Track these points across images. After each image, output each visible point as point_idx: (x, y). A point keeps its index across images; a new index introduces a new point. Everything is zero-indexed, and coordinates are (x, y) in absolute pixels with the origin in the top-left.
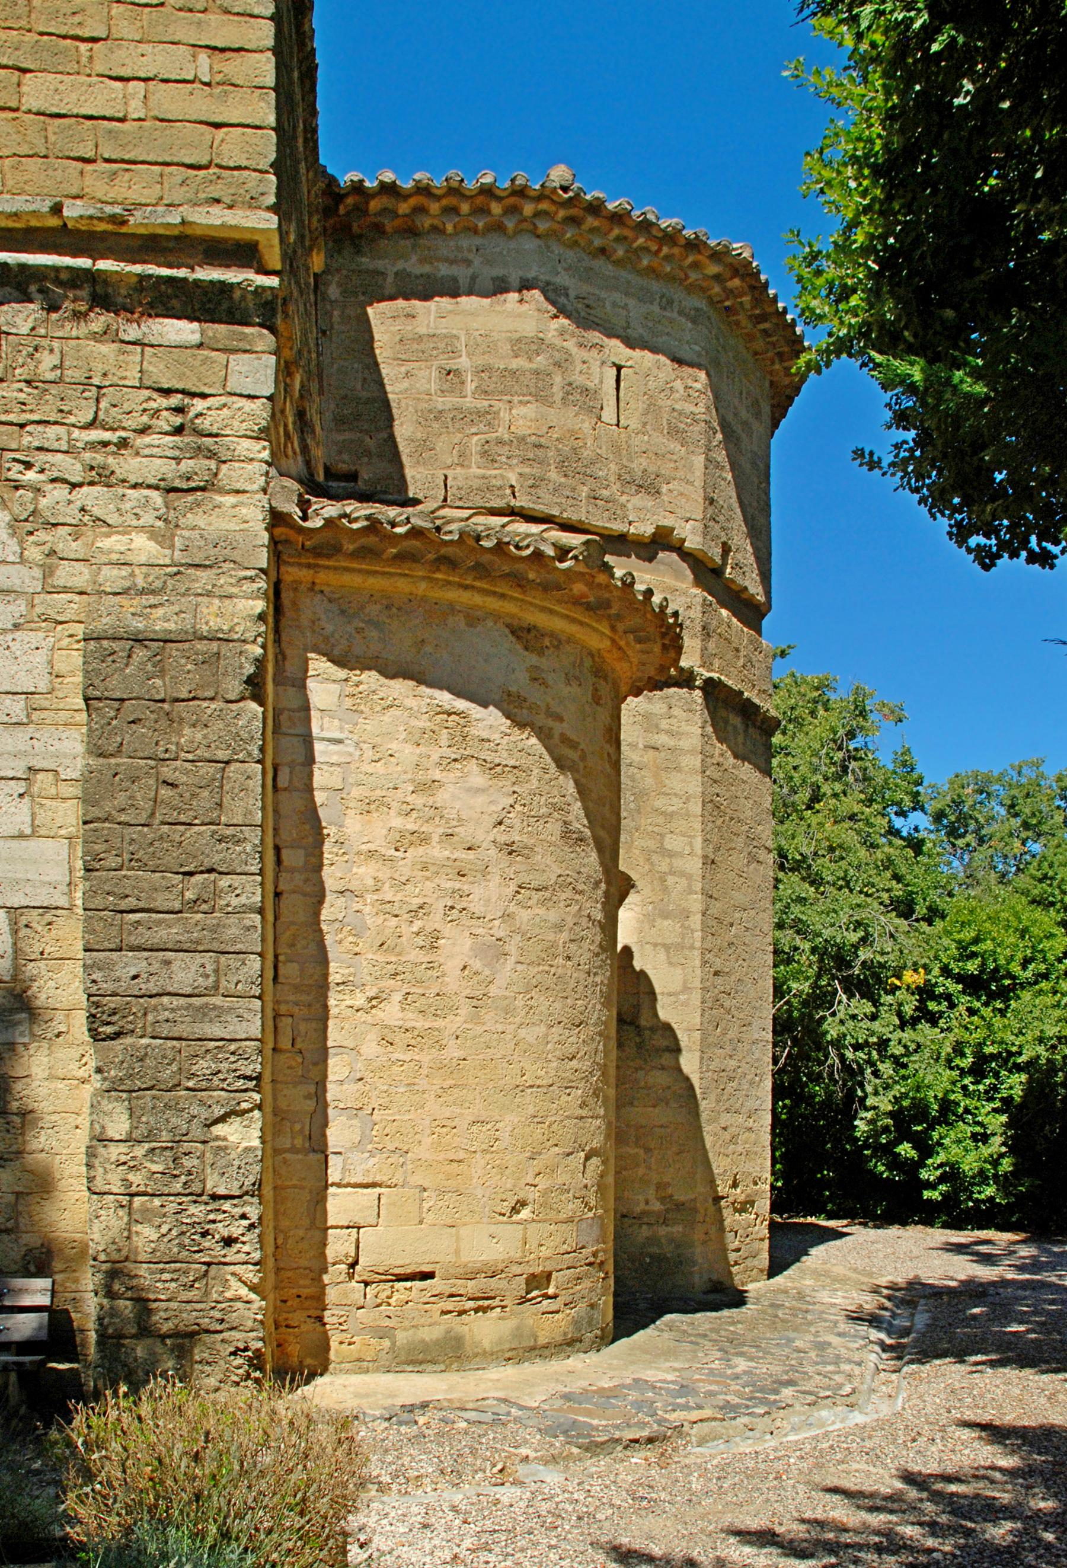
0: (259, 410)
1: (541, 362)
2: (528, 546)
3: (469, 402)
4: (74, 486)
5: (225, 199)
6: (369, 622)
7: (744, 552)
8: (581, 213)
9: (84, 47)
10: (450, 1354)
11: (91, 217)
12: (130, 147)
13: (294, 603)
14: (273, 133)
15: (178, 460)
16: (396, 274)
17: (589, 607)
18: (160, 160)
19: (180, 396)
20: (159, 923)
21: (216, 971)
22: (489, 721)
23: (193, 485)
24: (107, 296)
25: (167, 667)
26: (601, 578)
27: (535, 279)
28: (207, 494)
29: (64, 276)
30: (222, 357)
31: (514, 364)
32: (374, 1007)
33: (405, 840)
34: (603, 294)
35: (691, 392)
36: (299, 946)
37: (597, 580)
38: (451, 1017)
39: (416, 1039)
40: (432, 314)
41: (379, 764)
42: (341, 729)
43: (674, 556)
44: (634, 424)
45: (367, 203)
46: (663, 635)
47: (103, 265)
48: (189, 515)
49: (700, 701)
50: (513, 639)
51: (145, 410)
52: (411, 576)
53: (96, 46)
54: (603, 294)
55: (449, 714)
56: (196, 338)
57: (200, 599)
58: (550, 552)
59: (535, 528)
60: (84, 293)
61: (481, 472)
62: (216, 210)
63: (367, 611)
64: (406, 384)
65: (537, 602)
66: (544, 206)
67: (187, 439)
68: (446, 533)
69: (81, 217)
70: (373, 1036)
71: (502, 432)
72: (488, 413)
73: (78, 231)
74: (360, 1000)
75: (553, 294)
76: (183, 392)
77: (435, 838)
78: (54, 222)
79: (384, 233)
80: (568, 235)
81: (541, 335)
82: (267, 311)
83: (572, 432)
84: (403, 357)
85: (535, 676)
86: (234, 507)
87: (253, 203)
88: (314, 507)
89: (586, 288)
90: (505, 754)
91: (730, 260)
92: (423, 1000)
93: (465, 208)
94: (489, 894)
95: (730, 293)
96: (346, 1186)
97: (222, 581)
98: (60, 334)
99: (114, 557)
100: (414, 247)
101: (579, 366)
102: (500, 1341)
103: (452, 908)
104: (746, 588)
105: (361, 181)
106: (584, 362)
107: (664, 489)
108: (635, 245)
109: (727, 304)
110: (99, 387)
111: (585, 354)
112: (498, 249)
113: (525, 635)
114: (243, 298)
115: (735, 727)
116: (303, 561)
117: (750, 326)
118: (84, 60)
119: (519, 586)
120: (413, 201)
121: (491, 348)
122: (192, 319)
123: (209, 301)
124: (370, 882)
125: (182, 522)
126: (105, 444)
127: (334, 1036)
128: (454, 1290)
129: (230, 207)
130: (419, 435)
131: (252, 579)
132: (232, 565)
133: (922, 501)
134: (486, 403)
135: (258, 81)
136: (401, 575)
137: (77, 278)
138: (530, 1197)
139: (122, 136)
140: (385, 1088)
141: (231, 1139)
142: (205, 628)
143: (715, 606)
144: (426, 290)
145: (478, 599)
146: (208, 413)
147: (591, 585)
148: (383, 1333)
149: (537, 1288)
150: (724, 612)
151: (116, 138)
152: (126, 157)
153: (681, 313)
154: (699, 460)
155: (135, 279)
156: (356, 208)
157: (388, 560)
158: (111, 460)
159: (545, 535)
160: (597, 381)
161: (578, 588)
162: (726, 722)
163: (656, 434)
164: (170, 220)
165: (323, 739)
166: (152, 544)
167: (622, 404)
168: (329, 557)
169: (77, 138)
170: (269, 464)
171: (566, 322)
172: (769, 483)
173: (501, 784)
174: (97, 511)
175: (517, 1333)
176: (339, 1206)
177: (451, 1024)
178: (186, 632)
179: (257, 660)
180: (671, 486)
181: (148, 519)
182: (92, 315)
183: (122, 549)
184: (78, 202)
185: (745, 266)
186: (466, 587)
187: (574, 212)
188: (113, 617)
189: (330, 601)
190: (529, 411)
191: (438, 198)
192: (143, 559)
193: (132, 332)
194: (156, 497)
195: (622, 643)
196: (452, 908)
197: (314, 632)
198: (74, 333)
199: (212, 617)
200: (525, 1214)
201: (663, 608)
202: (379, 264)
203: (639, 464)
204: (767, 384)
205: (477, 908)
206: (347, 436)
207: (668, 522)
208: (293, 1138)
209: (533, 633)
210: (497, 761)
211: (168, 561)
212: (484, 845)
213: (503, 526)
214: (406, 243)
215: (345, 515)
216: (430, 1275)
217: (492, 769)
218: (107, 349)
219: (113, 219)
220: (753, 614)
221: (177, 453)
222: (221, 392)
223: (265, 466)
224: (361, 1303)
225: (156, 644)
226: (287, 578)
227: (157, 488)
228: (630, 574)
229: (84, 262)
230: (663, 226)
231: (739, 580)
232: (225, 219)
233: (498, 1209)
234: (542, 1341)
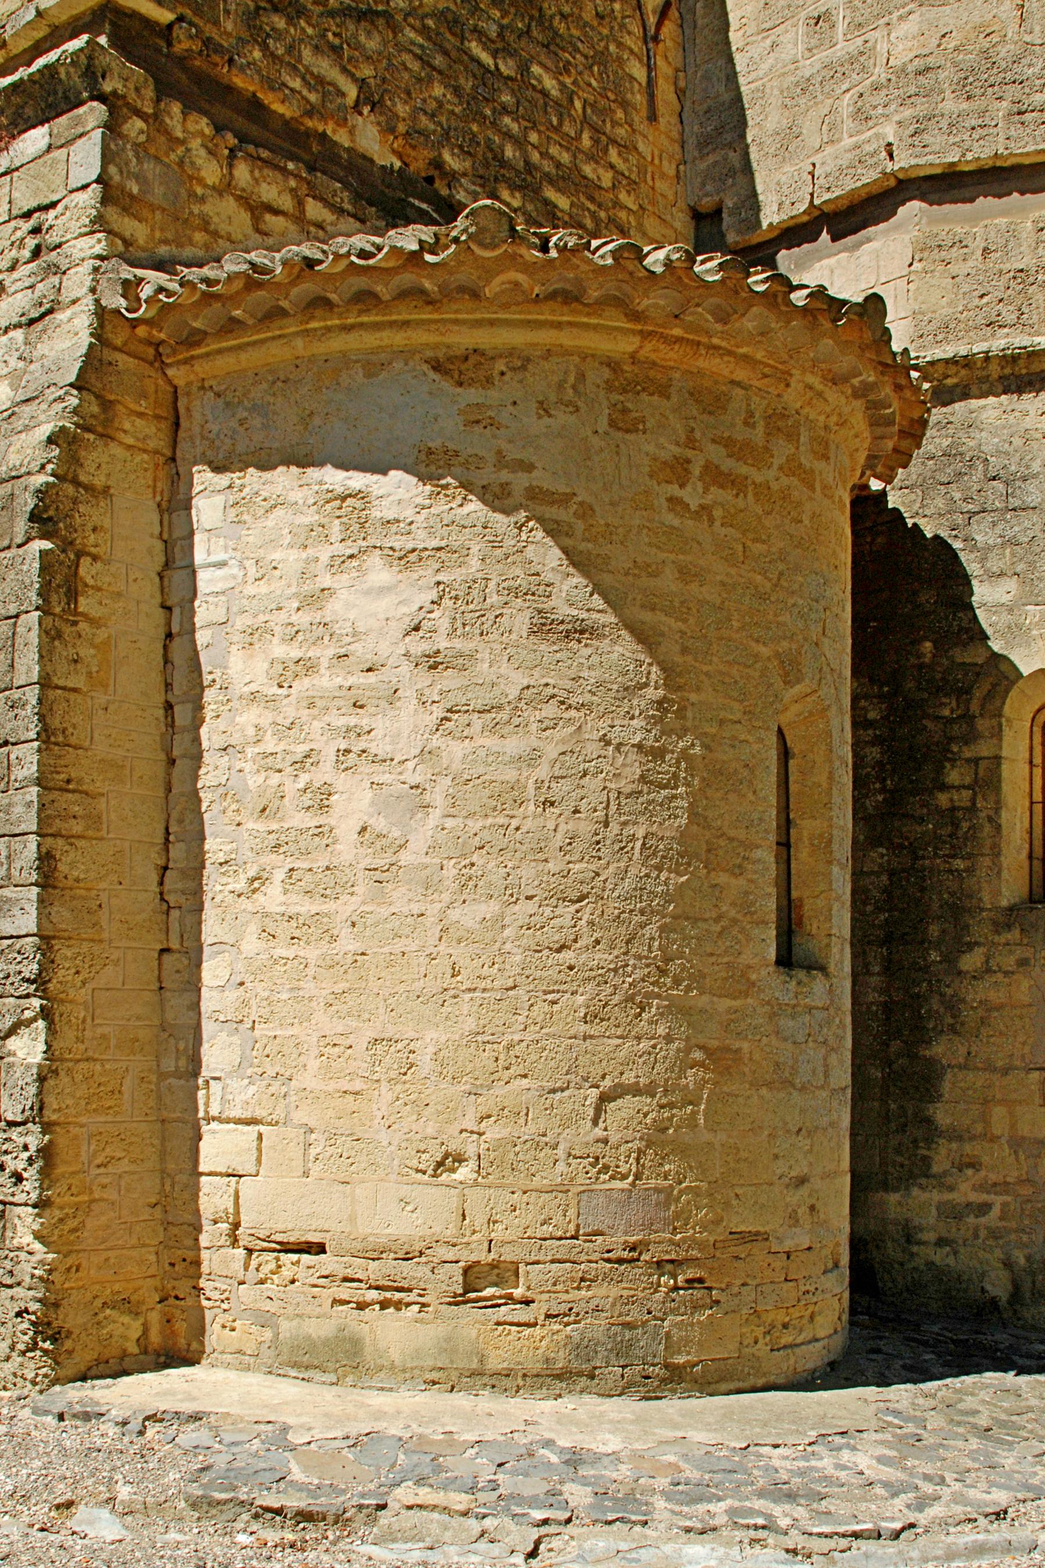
6: (254, 408)
10: (341, 1360)
13: (188, 409)
22: (396, 491)
32: (257, 889)
33: (286, 674)
36: (187, 821)
38: (344, 898)
39: (301, 928)
41: (262, 582)
55: (344, 499)
70: (253, 928)
71: (879, 73)
72: (862, 53)
74: (241, 885)
77: (324, 663)
83: (978, 28)
84: (767, 26)
86: (70, 320)
90: (421, 534)
92: (308, 876)
94: (400, 729)
96: (228, 1121)
102: (417, 1353)
103: (347, 751)
116: (181, 357)
124: (251, 731)
127: (212, 929)
128: (349, 1273)
138: (471, 1151)
140: (266, 994)
145: (371, 340)
148: (265, 1320)
149: (496, 1285)
165: (209, 565)
168: (198, 344)
173: (415, 576)
175: (448, 1346)
176: (217, 1147)
177: (346, 907)
186: (348, 329)
196: (347, 751)
200: (464, 1173)
205: (379, 746)
208: (177, 1059)
209: (472, 360)
210: (410, 546)
212: (391, 662)
216: (320, 1249)
217: (405, 559)
224: (241, 1276)
233: (414, 1163)
234: (494, 1363)
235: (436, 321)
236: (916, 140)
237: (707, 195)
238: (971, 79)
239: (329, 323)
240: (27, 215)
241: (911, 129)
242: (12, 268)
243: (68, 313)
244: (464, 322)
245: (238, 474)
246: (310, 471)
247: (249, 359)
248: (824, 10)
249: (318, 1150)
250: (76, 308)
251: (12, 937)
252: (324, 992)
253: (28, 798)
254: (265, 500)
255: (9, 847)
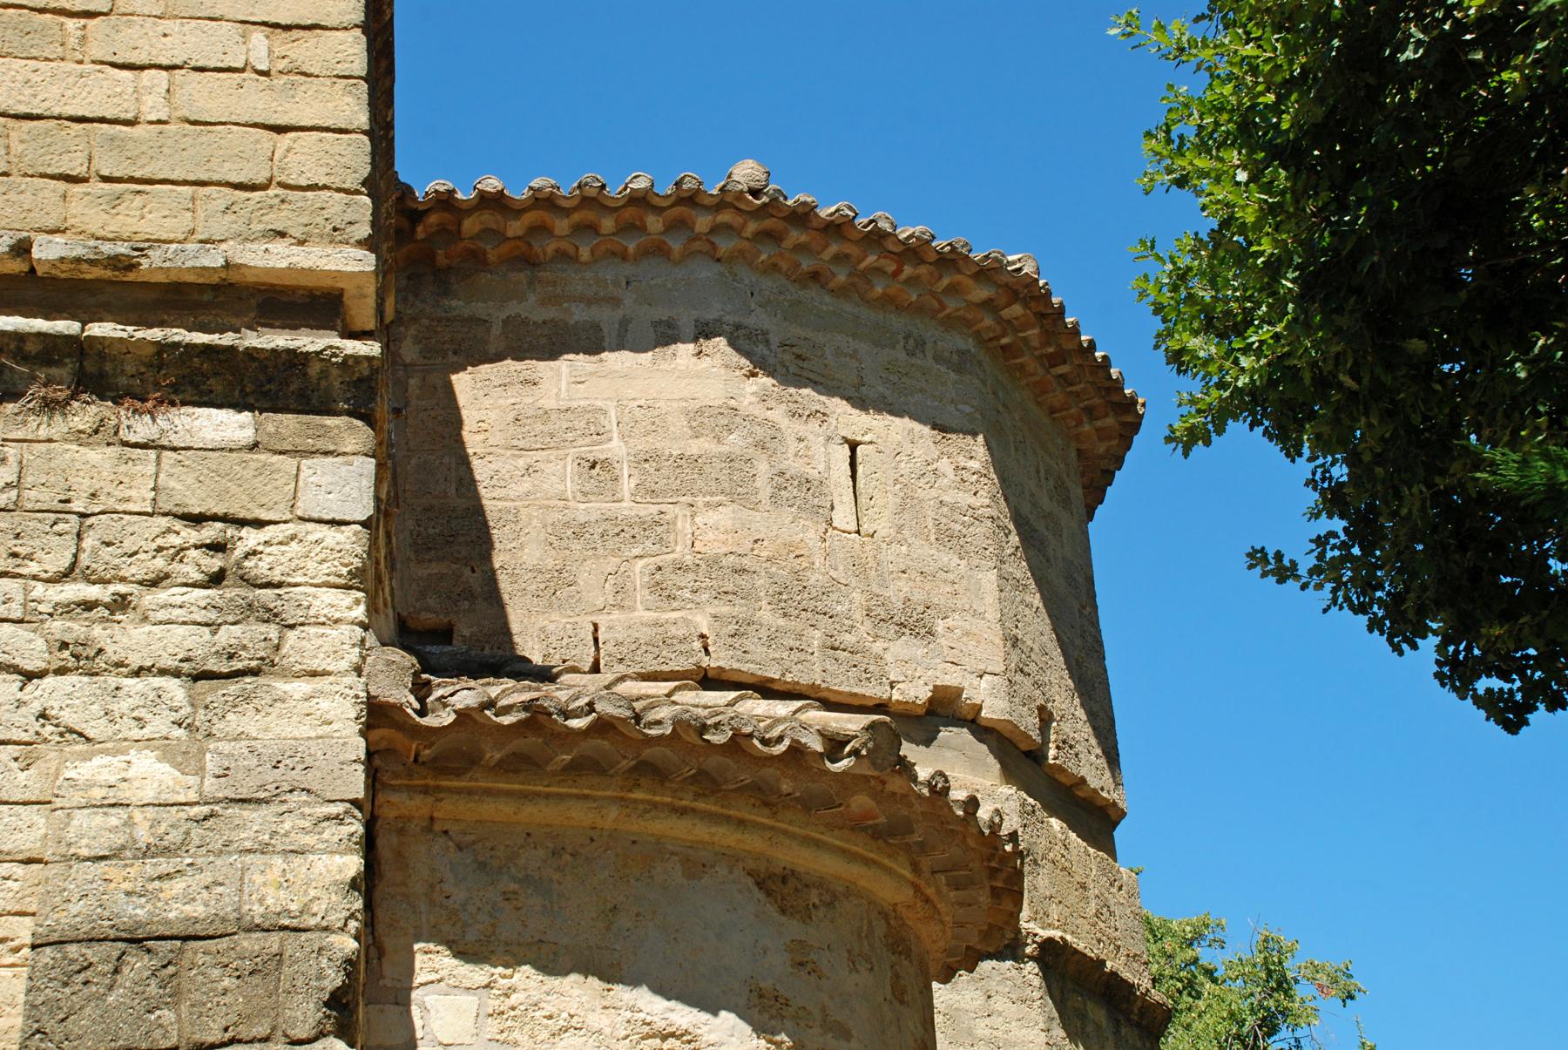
0: (349, 545)
1: (735, 442)
2: (780, 739)
3: (626, 508)
4: (29, 676)
5: (292, 231)
6: (526, 880)
7: (1073, 723)
8: (780, 225)
9: (71, 24)
11: (78, 260)
12: (144, 160)
13: (399, 855)
14: (365, 139)
15: (213, 626)
16: (506, 322)
17: (877, 834)
18: (192, 177)
19: (219, 525)
23: (238, 665)
24: (102, 375)
25: (185, 985)
26: (896, 784)
27: (719, 321)
28: (261, 680)
29: (31, 347)
30: (289, 463)
31: (694, 447)
34: (820, 338)
35: (966, 475)
37: (890, 787)
40: (564, 379)
43: (965, 734)
44: (884, 528)
45: (460, 224)
46: (993, 873)
47: (97, 329)
48: (230, 716)
49: (1037, 981)
50: (760, 895)
51: (160, 549)
52: (594, 799)
53: (91, 23)
54: (820, 338)
55: (664, 1038)
56: (247, 436)
57: (249, 858)
58: (817, 746)
59: (782, 708)
60: (64, 372)
61: (653, 615)
62: (278, 247)
63: (521, 862)
64: (526, 485)
65: (796, 830)
66: (725, 217)
67: (230, 592)
68: (650, 725)
69: (62, 259)
71: (681, 552)
73: (54, 279)
75: (742, 341)
76: (225, 519)
78: (17, 266)
79: (485, 263)
80: (764, 257)
81: (733, 403)
82: (356, 393)
83: (790, 547)
84: (521, 444)
85: (799, 958)
87: (336, 235)
88: (438, 693)
89: (795, 331)
91: (1004, 279)
93: (608, 224)
95: (1008, 325)
97: (287, 826)
98: (20, 435)
99: (97, 794)
100: (530, 283)
101: (793, 446)
104: (1083, 780)
105: (451, 192)
106: (800, 440)
107: (940, 627)
108: (862, 266)
109: (1004, 341)
110: (83, 516)
111: (799, 427)
112: (659, 281)
113: (778, 886)
114: (324, 374)
115: (1098, 1027)
117: (1041, 371)
118: (72, 41)
119: (766, 804)
120: (529, 218)
121: (657, 426)
122: (239, 407)
123: (269, 381)
125: (218, 727)
126: (89, 606)
129: (301, 243)
130: (550, 563)
131: (338, 819)
132: (304, 797)
133: (1374, 625)
134: (654, 509)
135: (343, 69)
136: (578, 797)
137: (51, 350)
139: (130, 145)
142: (258, 909)
143: (1041, 814)
144: (550, 342)
145: (702, 831)
146: (265, 551)
147: (875, 795)
150: (1055, 823)
151: (121, 148)
152: (137, 174)
153: (938, 358)
154: (989, 579)
155: (151, 350)
156: (442, 229)
157: (554, 774)
158: (97, 630)
159: (803, 717)
160: (821, 467)
161: (860, 802)
162: (1083, 1016)
163: (918, 542)
164: (207, 262)
166: (166, 767)
167: (863, 500)
168: (458, 773)
169: (58, 148)
170: (365, 627)
171: (769, 381)
172: (1095, 607)
174: (68, 717)
178: (224, 920)
179: (348, 961)
180: (949, 622)
181: (159, 725)
182: (76, 404)
183: (112, 779)
184: (58, 238)
185: (1027, 286)
186: (683, 812)
187: (768, 223)
188: (92, 900)
189: (460, 848)
190: (724, 517)
191: (567, 212)
192: (149, 795)
193: (143, 428)
194: (175, 689)
195: (930, 891)
197: (432, 903)
198: (43, 433)
199: (270, 889)
201: (994, 827)
202: (479, 309)
203: (897, 591)
204: (1073, 454)
206: (434, 568)
207: (951, 679)
209: (792, 883)
211: (192, 796)
213: (731, 704)
214: (522, 277)
215: (491, 704)
218: (100, 456)
219: (115, 262)
220: (1096, 820)
221: (212, 615)
222: (288, 516)
223: (359, 630)
225: (168, 944)
226: (388, 813)
227: (176, 674)
228: (941, 774)
229: (66, 326)
230: (902, 236)
231: (1071, 766)
232: (294, 260)
235: (772, 828)
236: (737, 642)
237: (428, 609)
238: (785, 597)
239: (658, 798)
241: (732, 628)
244: (793, 836)
245: (500, 969)
246: (619, 989)
247: (535, 813)
248: (602, 457)
254: (550, 1017)
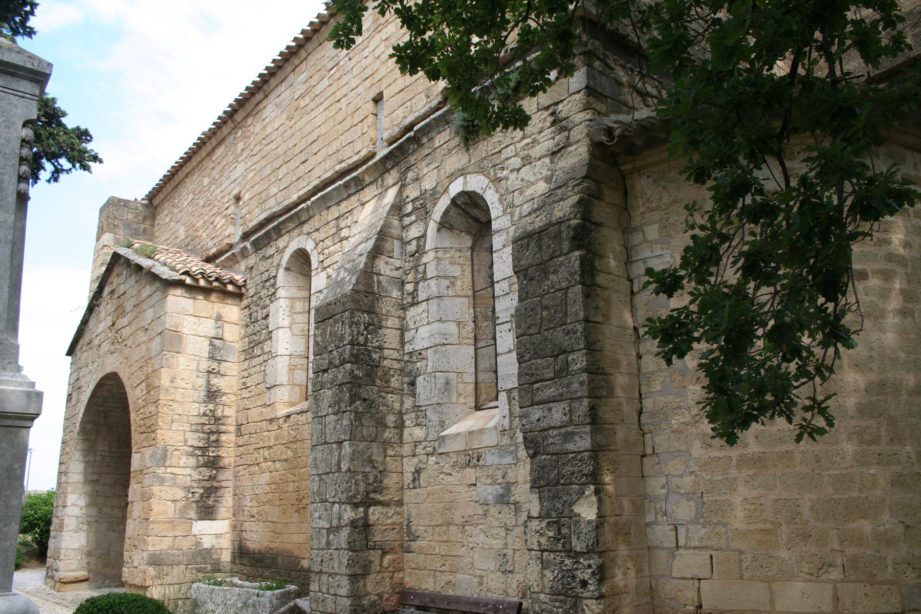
4: (519, 170)
15: (553, 138)
20: (546, 386)
21: (570, 411)
42: (662, 249)
141: (582, 515)
240: (547, 108)
242: (540, 132)
243: (575, 147)
249: (748, 564)
250: (579, 144)
251: (574, 452)
252: (743, 475)
253: (581, 379)
255: (570, 405)
